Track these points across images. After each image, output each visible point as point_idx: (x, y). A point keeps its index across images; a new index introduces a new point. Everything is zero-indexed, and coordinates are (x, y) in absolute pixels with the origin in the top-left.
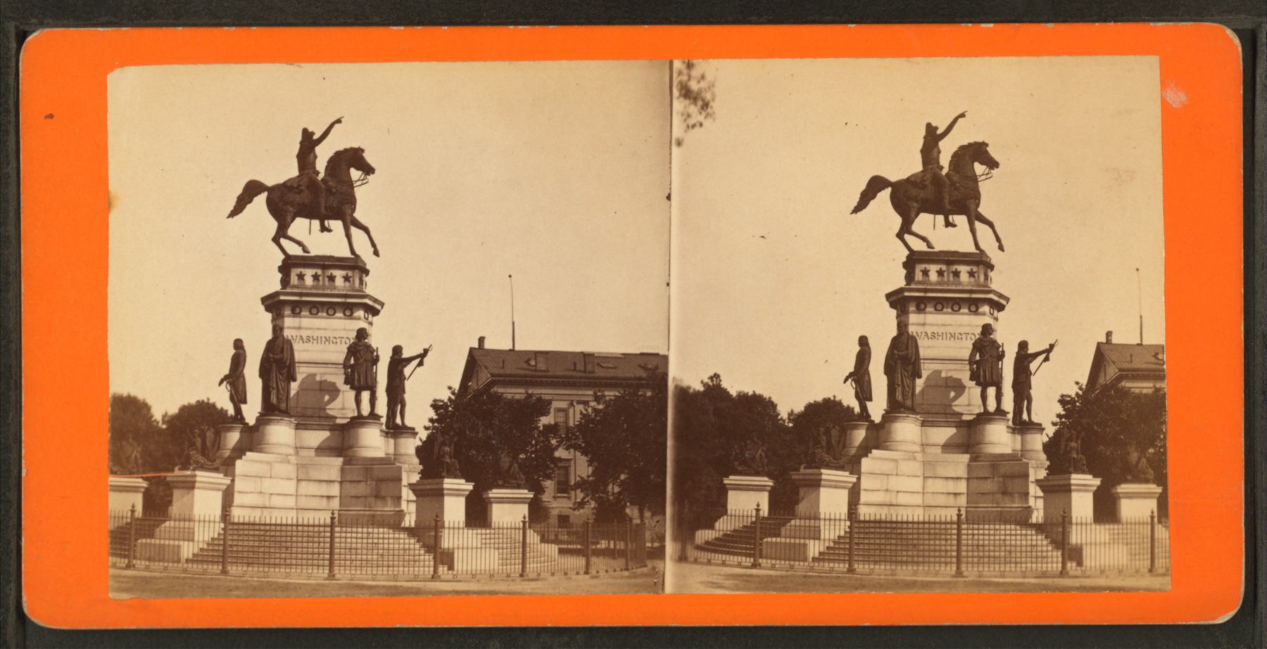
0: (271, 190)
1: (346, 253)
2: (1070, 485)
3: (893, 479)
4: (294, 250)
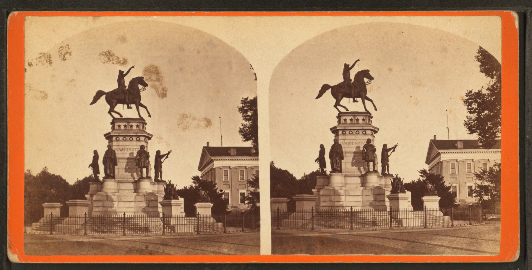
1: (363, 110)
2: (171, 204)
3: (106, 203)
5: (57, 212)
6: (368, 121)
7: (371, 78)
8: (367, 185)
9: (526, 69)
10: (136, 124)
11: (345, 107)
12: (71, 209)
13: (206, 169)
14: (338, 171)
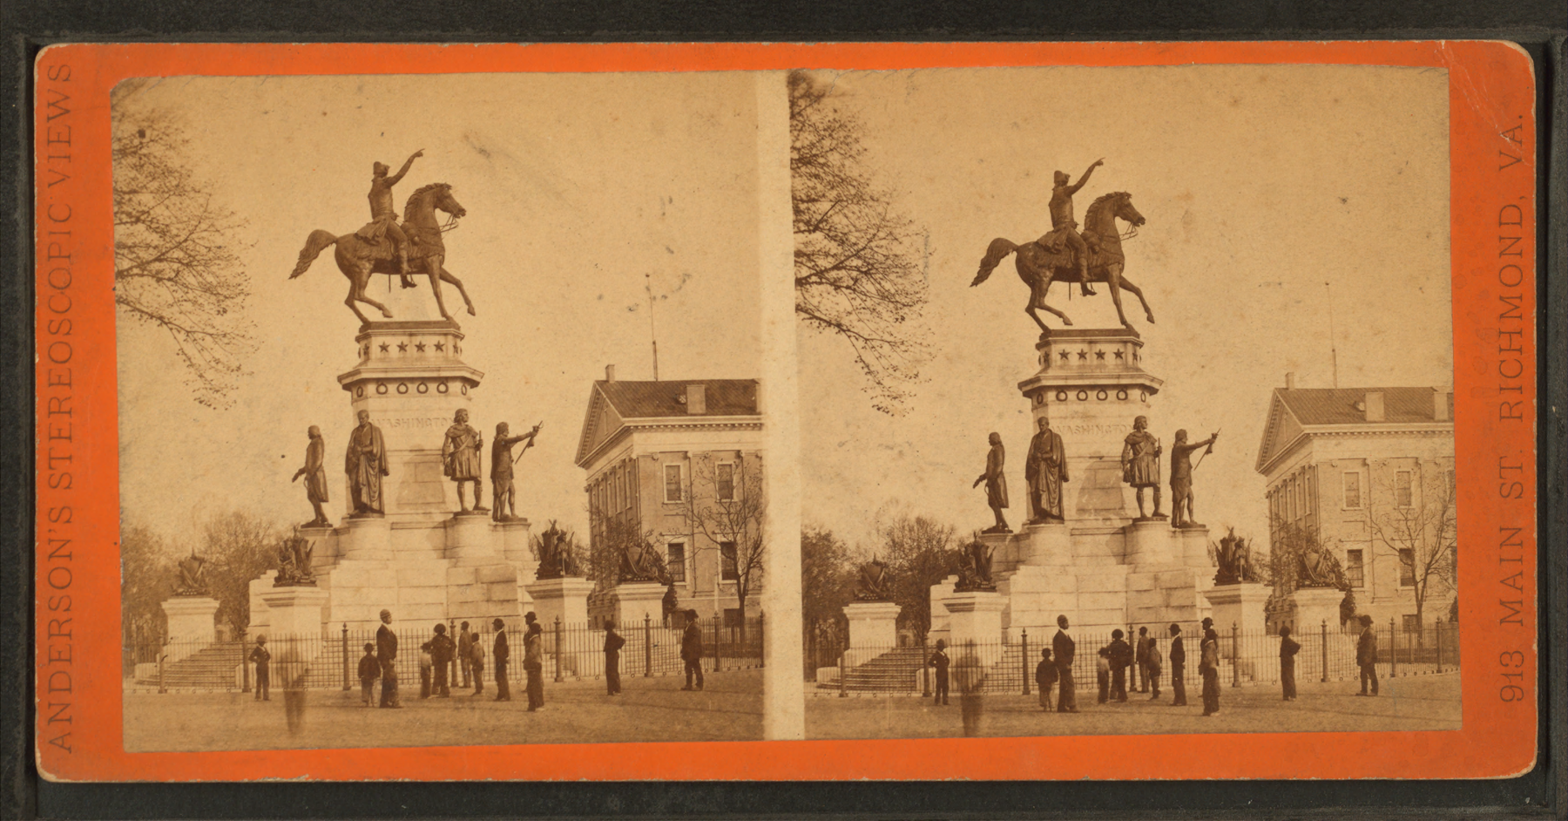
0: (336, 241)
1: (1119, 326)
6: (1130, 358)
9: (1551, 211)
11: (1060, 315)
14: (1054, 517)
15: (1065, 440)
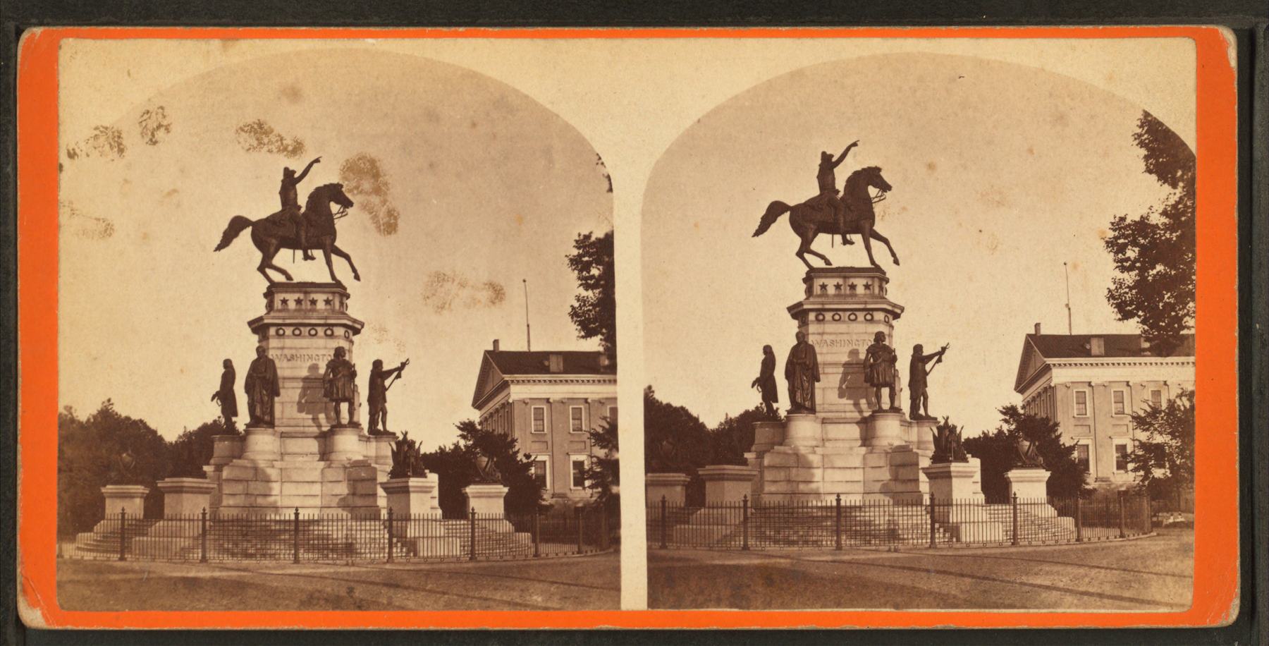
1: (867, 264)
3: (252, 485)
4: (817, 263)
5: (135, 508)
6: (877, 291)
7: (885, 187)
8: (875, 442)
9: (1255, 166)
10: (324, 297)
11: (822, 257)
12: (168, 499)
13: (491, 404)
14: (807, 409)
15: (817, 349)
